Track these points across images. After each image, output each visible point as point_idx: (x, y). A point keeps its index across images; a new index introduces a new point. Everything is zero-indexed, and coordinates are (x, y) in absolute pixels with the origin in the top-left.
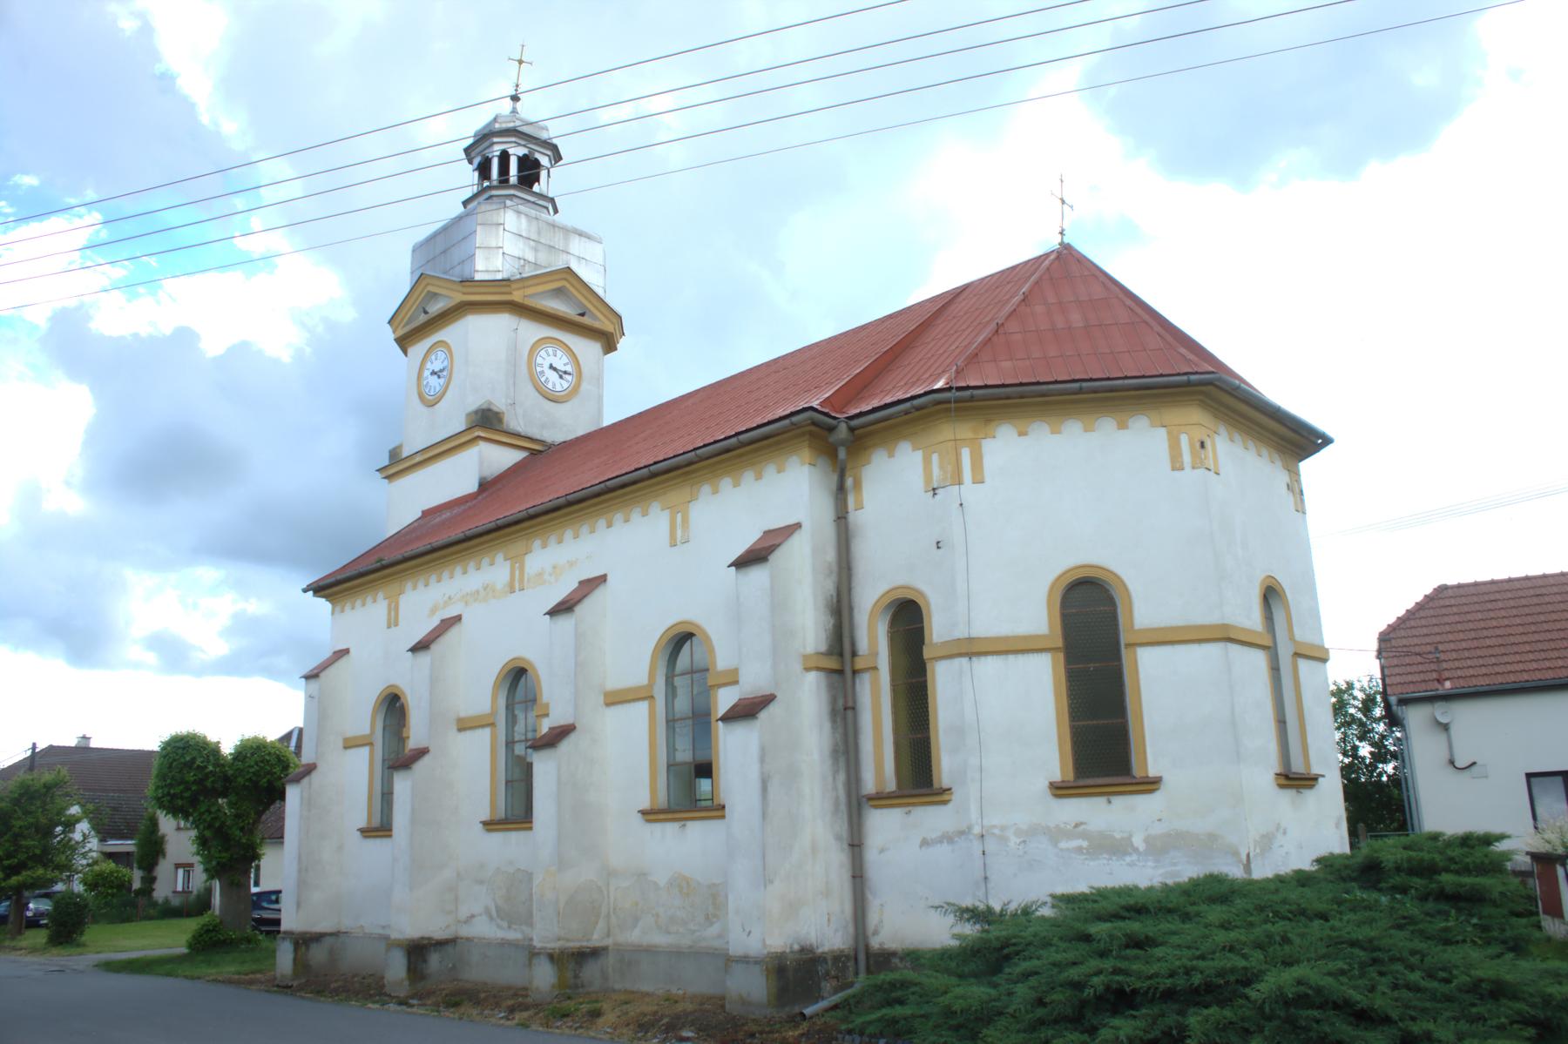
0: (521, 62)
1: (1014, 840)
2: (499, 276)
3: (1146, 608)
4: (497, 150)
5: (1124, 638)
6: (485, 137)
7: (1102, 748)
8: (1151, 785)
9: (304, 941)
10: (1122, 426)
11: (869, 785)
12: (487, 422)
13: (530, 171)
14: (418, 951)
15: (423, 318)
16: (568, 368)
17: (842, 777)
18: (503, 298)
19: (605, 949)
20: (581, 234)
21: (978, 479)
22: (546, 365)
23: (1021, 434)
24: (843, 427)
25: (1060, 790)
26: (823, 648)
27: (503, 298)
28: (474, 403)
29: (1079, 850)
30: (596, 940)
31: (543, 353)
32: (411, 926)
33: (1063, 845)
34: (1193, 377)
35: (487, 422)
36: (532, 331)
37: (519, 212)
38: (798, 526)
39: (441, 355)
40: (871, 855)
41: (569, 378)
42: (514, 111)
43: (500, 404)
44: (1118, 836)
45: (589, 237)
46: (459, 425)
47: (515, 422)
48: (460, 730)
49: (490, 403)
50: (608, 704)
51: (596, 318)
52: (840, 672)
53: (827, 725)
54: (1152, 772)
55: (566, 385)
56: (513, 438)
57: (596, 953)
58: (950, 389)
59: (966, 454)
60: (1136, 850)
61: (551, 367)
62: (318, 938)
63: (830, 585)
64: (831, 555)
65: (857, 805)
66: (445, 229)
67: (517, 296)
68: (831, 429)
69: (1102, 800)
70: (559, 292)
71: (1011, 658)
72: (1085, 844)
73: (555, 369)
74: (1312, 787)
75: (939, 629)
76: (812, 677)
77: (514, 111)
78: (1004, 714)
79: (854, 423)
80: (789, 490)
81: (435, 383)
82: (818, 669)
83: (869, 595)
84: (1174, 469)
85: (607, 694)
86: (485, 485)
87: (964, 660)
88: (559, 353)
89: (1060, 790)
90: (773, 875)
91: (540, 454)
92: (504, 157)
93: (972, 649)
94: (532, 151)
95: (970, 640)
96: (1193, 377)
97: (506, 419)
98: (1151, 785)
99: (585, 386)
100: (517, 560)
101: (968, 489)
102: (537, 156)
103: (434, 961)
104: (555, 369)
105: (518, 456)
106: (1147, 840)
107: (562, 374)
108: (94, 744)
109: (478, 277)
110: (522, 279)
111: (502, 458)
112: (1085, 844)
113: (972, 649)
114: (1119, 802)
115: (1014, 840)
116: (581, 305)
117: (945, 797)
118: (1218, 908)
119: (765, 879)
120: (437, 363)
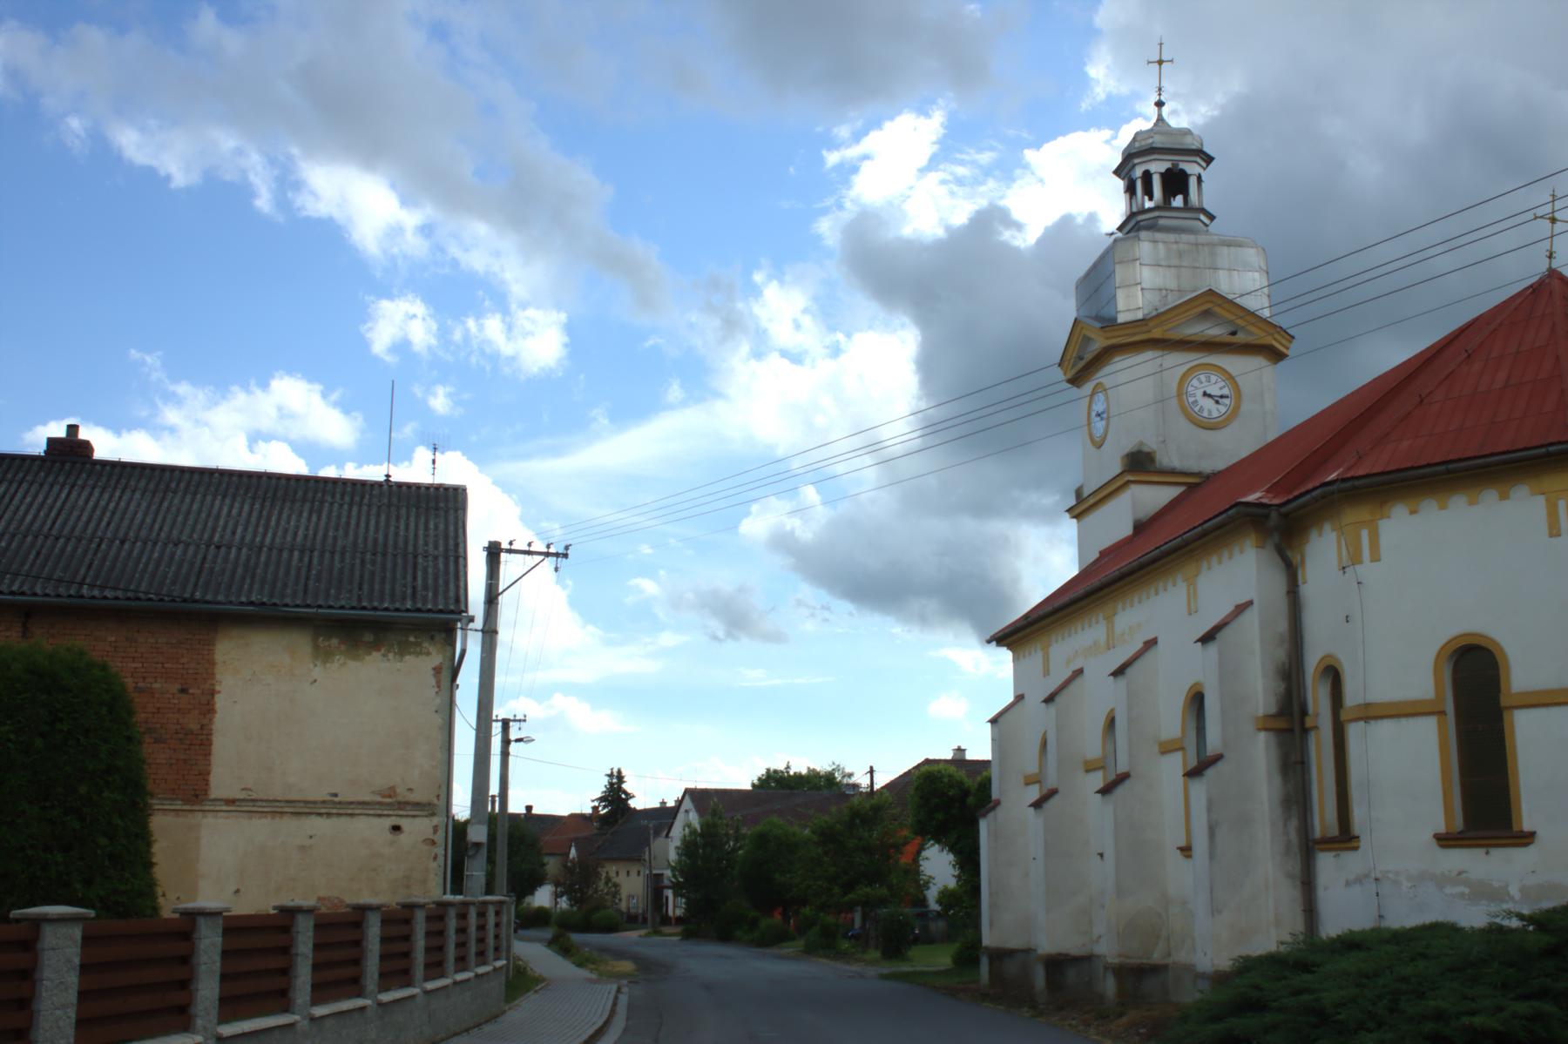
0: (1160, 62)
1: (1406, 884)
2: (1140, 315)
3: (1521, 676)
4: (1138, 172)
5: (1504, 701)
6: (1130, 157)
7: (1485, 805)
8: (1526, 839)
9: (1000, 955)
10: (1504, 496)
11: (1318, 833)
12: (1140, 464)
13: (1176, 182)
14: (1057, 964)
15: (1081, 364)
16: (1226, 391)
17: (1294, 823)
18: (1149, 336)
19: (1165, 967)
20: (1229, 244)
21: (1376, 557)
22: (1199, 393)
23: (1412, 512)
24: (1274, 515)
25: (1445, 840)
26: (1273, 710)
27: (1149, 336)
28: (1128, 445)
29: (1462, 895)
30: (1157, 957)
31: (1195, 382)
32: (1047, 944)
33: (1448, 890)
34: (1551, 449)
35: (1140, 464)
36: (1177, 362)
37: (1155, 242)
38: (1250, 603)
39: (1101, 396)
40: (1321, 894)
41: (1227, 401)
42: (1160, 119)
43: (1151, 444)
44: (1496, 884)
45: (1240, 245)
46: (1117, 468)
47: (1169, 458)
48: (1088, 771)
49: (1141, 443)
50: (1163, 753)
51: (1251, 333)
52: (1291, 731)
53: (1277, 780)
54: (1527, 826)
55: (1223, 409)
56: (1169, 475)
57: (1156, 969)
58: (1344, 480)
59: (1365, 534)
60: (1512, 898)
61: (1205, 394)
62: (1011, 953)
63: (1281, 654)
64: (1282, 625)
65: (1308, 848)
66: (1095, 267)
67: (1157, 333)
68: (1267, 516)
69: (1480, 852)
70: (1206, 314)
71: (1404, 721)
72: (1467, 891)
73: (1210, 396)
74: (1526, 845)
75: (1353, 695)
76: (1262, 735)
77: (1160, 119)
78: (1402, 771)
79: (1284, 510)
80: (1239, 575)
81: (1099, 426)
82: (1266, 729)
83: (1312, 662)
84: (1551, 536)
85: (1086, 763)
86: (1140, 527)
87: (1362, 723)
88: (1213, 379)
89: (1445, 840)
90: (1224, 909)
91: (1196, 485)
92: (1147, 176)
93: (1371, 713)
94: (1175, 165)
95: (1367, 705)
96: (1551, 449)
97: (1158, 457)
98: (1526, 839)
99: (1245, 407)
100: (1109, 619)
101: (1366, 569)
102: (1182, 166)
103: (1071, 975)
104: (1210, 396)
105: (1173, 492)
106: (1523, 890)
107: (1217, 400)
108: (969, 756)
109: (1121, 318)
110: (1158, 316)
111: (1153, 497)
112: (1467, 891)
113: (1371, 713)
114: (1498, 854)
115: (1406, 884)
116: (1231, 322)
117: (1354, 844)
118: (483, 881)
119: (1215, 911)
120: (1099, 406)
